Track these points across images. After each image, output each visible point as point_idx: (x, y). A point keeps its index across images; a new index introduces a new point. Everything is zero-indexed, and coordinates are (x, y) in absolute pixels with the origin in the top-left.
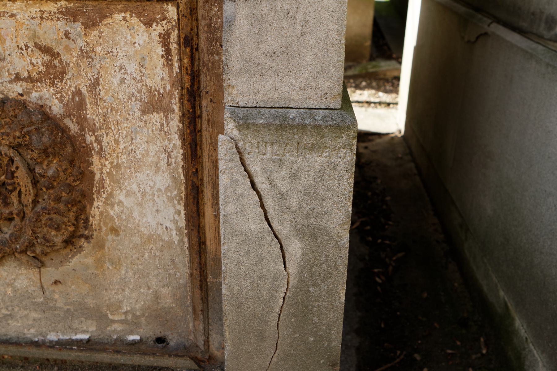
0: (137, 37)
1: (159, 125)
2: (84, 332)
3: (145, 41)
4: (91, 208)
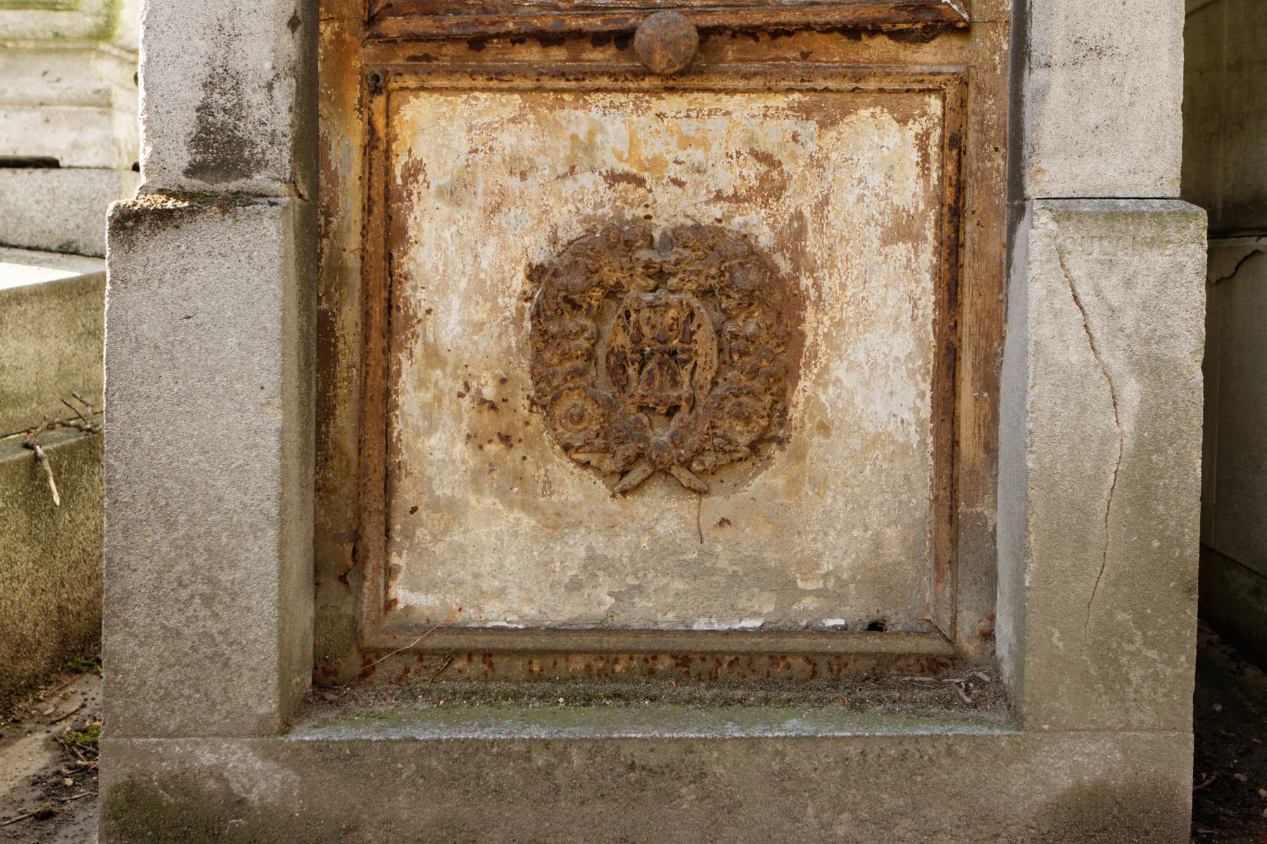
0: (886, 138)
1: (904, 260)
2: (755, 615)
3: (896, 144)
4: (793, 392)
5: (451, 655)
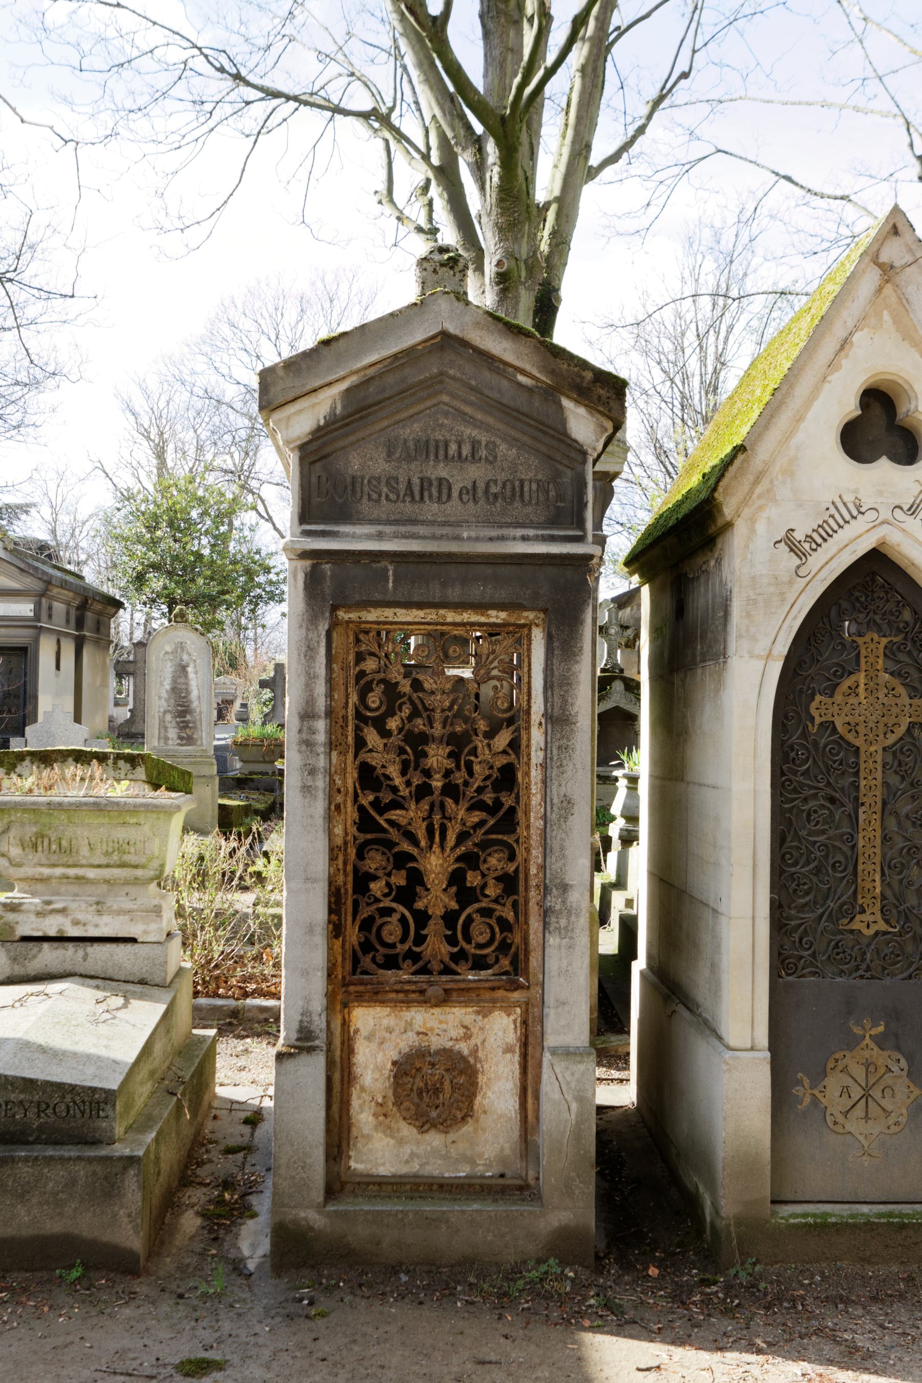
5: (368, 1184)
